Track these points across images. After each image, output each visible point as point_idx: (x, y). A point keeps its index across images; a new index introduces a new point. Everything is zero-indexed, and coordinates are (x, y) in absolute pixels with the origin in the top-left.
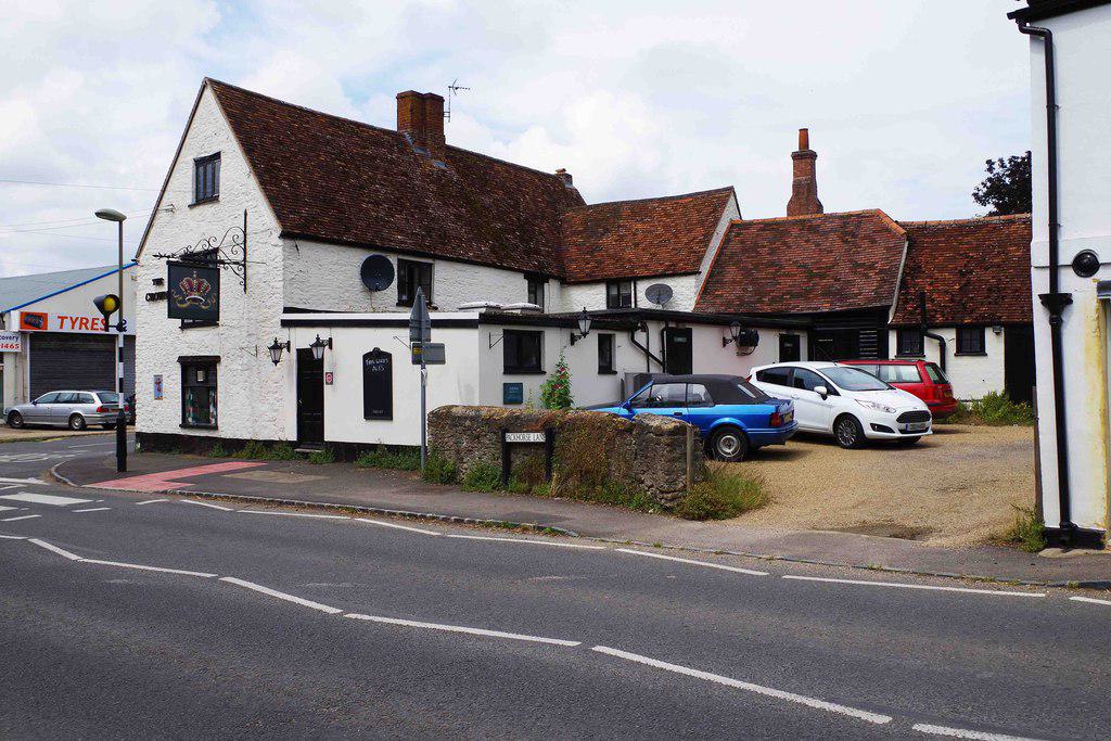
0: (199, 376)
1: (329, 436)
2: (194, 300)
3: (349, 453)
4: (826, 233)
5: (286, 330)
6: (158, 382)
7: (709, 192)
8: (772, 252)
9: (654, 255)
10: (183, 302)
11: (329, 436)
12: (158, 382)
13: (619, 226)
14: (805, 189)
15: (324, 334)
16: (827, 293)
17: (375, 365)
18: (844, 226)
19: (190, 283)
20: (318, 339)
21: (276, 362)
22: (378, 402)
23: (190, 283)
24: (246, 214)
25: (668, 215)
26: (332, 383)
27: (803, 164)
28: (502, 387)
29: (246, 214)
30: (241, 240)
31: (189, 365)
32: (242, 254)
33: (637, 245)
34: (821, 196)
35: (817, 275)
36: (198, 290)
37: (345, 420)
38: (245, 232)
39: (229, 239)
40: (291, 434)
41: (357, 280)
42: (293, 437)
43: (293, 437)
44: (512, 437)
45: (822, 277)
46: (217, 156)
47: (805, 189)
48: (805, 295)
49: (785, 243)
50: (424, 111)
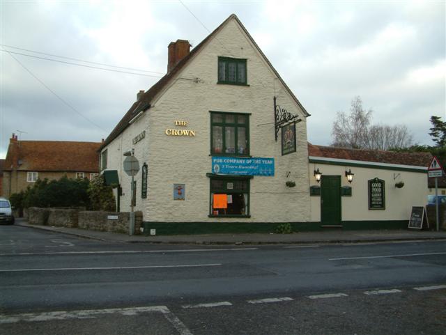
1: (344, 218)
5: (312, 166)
6: (179, 191)
11: (344, 218)
15: (348, 169)
22: (377, 202)
24: (275, 99)
37: (354, 209)
42: (318, 219)
43: (318, 219)
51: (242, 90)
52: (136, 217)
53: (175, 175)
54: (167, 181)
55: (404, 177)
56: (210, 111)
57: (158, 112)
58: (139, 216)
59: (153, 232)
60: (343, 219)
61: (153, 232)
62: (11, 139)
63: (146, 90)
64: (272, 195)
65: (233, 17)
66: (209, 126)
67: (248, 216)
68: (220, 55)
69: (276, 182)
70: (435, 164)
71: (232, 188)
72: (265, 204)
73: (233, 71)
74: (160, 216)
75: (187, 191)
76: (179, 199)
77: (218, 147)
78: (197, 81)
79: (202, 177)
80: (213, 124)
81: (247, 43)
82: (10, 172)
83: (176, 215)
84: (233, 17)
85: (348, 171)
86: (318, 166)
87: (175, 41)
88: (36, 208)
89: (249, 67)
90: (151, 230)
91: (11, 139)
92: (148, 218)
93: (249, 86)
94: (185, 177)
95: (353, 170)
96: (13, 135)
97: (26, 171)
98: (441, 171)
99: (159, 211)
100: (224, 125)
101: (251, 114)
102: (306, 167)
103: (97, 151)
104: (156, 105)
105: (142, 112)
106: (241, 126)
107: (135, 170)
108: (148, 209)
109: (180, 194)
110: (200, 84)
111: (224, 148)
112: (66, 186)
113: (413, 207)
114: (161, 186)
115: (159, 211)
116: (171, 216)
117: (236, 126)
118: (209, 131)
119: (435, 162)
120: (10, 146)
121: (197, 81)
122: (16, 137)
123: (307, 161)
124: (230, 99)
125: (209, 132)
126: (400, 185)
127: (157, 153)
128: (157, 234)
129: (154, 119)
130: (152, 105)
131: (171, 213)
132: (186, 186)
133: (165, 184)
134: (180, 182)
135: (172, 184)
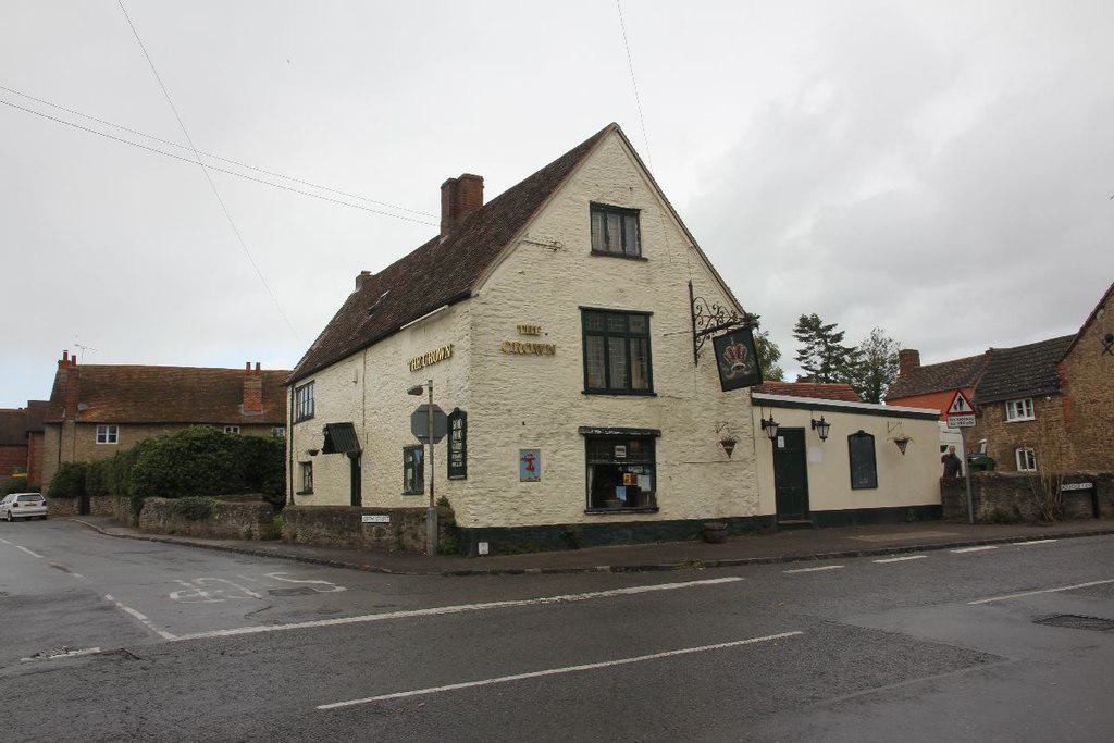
2: (738, 367)
5: (757, 410)
6: (530, 462)
10: (730, 373)
12: (530, 462)
15: (817, 416)
19: (730, 351)
21: (824, 438)
23: (730, 351)
24: (690, 286)
29: (690, 286)
37: (829, 487)
40: (768, 507)
44: (1065, 488)
51: (635, 267)
52: (439, 517)
53: (521, 432)
54: (506, 444)
55: (907, 427)
56: (580, 307)
57: (484, 307)
58: (444, 509)
59: (483, 548)
60: (812, 509)
61: (483, 548)
62: (60, 362)
63: (374, 273)
64: (694, 468)
65: (614, 129)
66: (579, 336)
67: (656, 510)
68: (594, 199)
69: (700, 443)
70: (961, 405)
71: (617, 462)
72: (685, 488)
73: (618, 230)
74: (495, 515)
75: (544, 463)
76: (530, 480)
77: (599, 382)
78: (555, 248)
79: (572, 435)
80: (586, 333)
81: (638, 180)
82: (60, 425)
83: (527, 511)
84: (614, 129)
85: (767, 419)
86: (767, 413)
87: (456, 176)
88: (163, 501)
89: (643, 223)
90: (480, 544)
91: (60, 362)
92: (465, 520)
93: (646, 260)
94: (540, 435)
95: (829, 417)
96: (66, 355)
97: (96, 424)
98: (973, 416)
99: (493, 506)
100: (606, 335)
101: (651, 314)
102: (748, 413)
103: (275, 386)
104: (482, 292)
105: (446, 306)
106: (617, 335)
107: (33, 432)
108: (474, 503)
109: (531, 468)
110: (560, 254)
111: (629, 379)
112: (180, 453)
113: (853, 488)
114: (492, 450)
115: (493, 506)
116: (517, 515)
117: (627, 336)
118: (579, 344)
119: (960, 400)
120: (58, 374)
121: (555, 248)
122: (74, 357)
123: (749, 402)
124: (614, 286)
125: (581, 347)
126: (902, 443)
127: (487, 388)
128: (493, 549)
129: (479, 320)
130: (473, 294)
131: (515, 510)
132: (542, 453)
133: (504, 450)
134: (529, 445)
135: (516, 449)
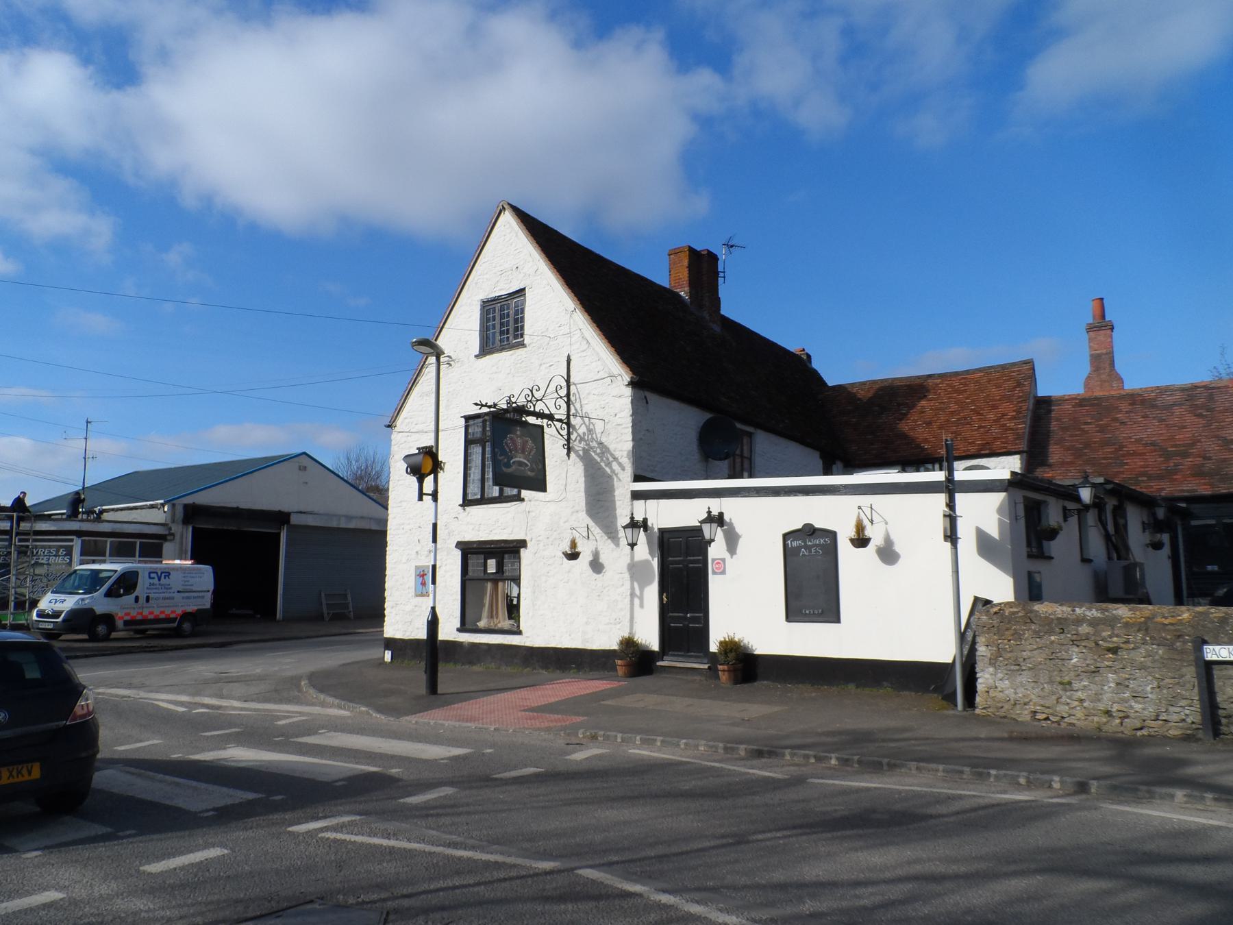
0: (491, 568)
3: (745, 666)
4: (1168, 408)
7: (1003, 367)
8: (1102, 429)
9: (956, 433)
13: (899, 405)
14: (1103, 362)
15: (715, 505)
16: (1198, 473)
17: (806, 547)
18: (1191, 398)
20: (709, 512)
25: (959, 392)
26: (723, 572)
27: (1101, 336)
28: (109, 599)
30: (563, 392)
31: (470, 551)
32: (564, 406)
33: (929, 424)
34: (1120, 367)
35: (1177, 454)
36: (523, 452)
38: (568, 381)
39: (552, 388)
41: (694, 447)
45: (1185, 455)
46: (521, 292)
47: (1103, 362)
48: (1167, 475)
49: (1116, 420)
50: (703, 267)
